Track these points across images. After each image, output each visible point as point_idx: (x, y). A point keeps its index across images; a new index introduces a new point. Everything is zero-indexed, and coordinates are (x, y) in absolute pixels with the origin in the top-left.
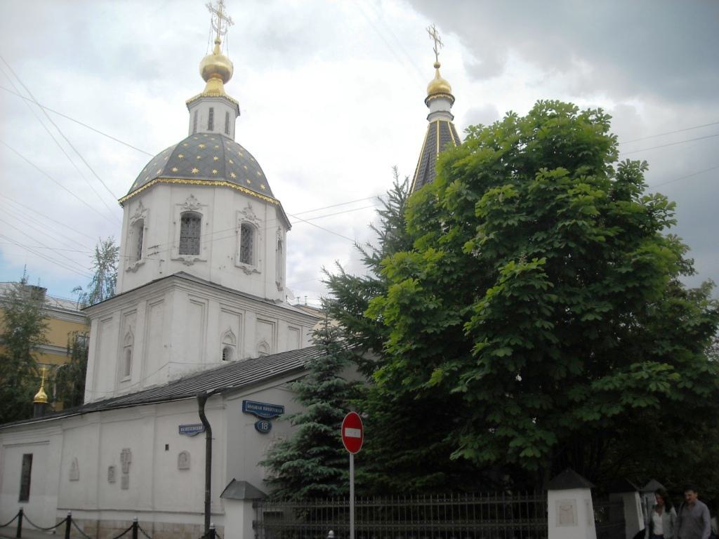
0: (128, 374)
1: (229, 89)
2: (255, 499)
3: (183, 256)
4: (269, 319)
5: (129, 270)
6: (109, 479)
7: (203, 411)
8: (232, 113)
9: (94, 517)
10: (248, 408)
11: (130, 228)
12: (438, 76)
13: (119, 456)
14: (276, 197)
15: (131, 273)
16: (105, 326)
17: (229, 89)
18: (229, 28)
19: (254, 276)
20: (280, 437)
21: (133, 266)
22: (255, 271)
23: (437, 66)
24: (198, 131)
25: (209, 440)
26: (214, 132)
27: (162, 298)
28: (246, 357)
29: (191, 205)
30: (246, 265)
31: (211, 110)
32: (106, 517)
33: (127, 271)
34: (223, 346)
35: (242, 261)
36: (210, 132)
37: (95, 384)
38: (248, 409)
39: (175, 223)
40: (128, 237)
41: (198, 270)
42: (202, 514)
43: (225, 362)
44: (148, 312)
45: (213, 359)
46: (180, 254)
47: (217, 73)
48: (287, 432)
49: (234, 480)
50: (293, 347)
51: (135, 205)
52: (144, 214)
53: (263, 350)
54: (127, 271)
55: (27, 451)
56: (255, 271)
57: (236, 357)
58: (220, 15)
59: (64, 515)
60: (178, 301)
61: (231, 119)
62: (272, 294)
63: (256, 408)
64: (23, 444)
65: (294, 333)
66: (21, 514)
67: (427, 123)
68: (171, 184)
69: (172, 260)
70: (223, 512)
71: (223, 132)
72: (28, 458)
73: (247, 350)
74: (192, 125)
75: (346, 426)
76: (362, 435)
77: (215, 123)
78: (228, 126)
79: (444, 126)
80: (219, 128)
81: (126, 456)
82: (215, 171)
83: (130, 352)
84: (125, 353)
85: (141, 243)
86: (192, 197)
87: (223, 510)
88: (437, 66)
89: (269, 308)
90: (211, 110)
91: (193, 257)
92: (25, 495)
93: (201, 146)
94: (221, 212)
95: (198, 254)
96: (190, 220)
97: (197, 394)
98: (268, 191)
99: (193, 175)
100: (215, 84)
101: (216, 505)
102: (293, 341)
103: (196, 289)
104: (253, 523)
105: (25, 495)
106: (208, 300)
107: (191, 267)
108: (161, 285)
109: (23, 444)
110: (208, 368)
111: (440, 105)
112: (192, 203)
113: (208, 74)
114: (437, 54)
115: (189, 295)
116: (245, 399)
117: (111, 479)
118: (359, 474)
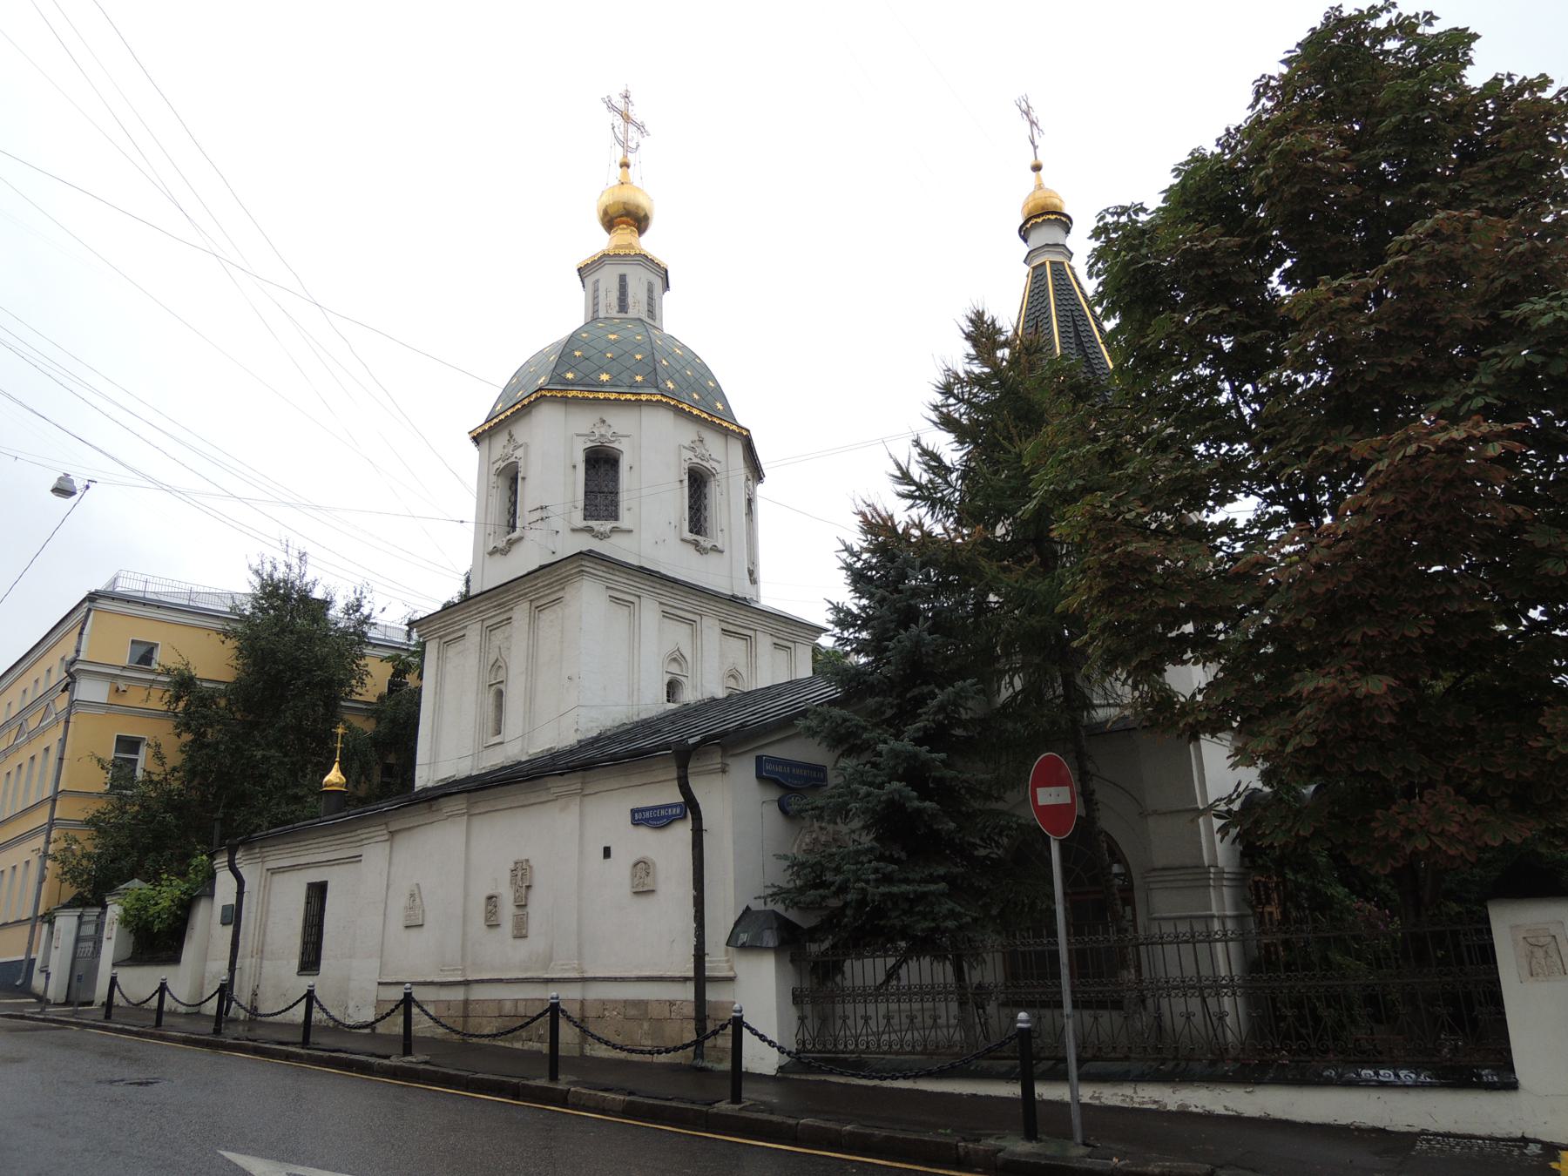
0: (498, 732)
1: (648, 243)
3: (595, 524)
4: (740, 631)
5: (495, 551)
7: (686, 777)
8: (658, 283)
9: (458, 995)
10: (767, 774)
11: (494, 478)
12: (1040, 187)
13: (508, 875)
14: (741, 422)
15: (498, 557)
16: (452, 652)
17: (648, 243)
18: (643, 142)
19: (713, 556)
21: (501, 544)
22: (715, 549)
23: (1037, 168)
24: (602, 314)
25: (698, 833)
28: (707, 695)
30: (699, 538)
31: (623, 278)
32: (478, 993)
33: (491, 554)
34: (667, 678)
35: (691, 531)
36: (622, 315)
40: (488, 495)
41: (615, 548)
42: (686, 979)
43: (672, 706)
44: (533, 621)
45: (651, 702)
47: (627, 217)
49: (748, 908)
50: (783, 678)
51: (501, 441)
52: (519, 453)
53: (732, 683)
54: (491, 554)
55: (315, 876)
56: (715, 549)
57: (689, 695)
58: (626, 118)
59: (397, 994)
60: (588, 600)
61: (656, 295)
62: (742, 589)
63: (780, 769)
64: (307, 866)
65: (783, 654)
67: (1027, 269)
68: (565, 401)
69: (574, 530)
70: (731, 974)
71: (644, 316)
72: (317, 893)
73: (706, 683)
75: (1037, 784)
76: (1073, 798)
77: (630, 300)
78: (652, 310)
80: (637, 308)
81: (522, 875)
82: (639, 378)
83: (500, 694)
84: (490, 698)
85: (514, 504)
86: (604, 422)
87: (731, 969)
89: (740, 612)
90: (623, 278)
91: (609, 525)
92: (310, 960)
93: (612, 337)
94: (654, 451)
95: (616, 518)
97: (661, 753)
98: (728, 413)
99: (603, 384)
100: (624, 236)
101: (718, 959)
102: (773, 668)
103: (620, 579)
105: (310, 960)
107: (606, 542)
108: (547, 581)
109: (307, 866)
110: (644, 716)
111: (1041, 237)
113: (611, 221)
114: (1035, 148)
116: (759, 753)
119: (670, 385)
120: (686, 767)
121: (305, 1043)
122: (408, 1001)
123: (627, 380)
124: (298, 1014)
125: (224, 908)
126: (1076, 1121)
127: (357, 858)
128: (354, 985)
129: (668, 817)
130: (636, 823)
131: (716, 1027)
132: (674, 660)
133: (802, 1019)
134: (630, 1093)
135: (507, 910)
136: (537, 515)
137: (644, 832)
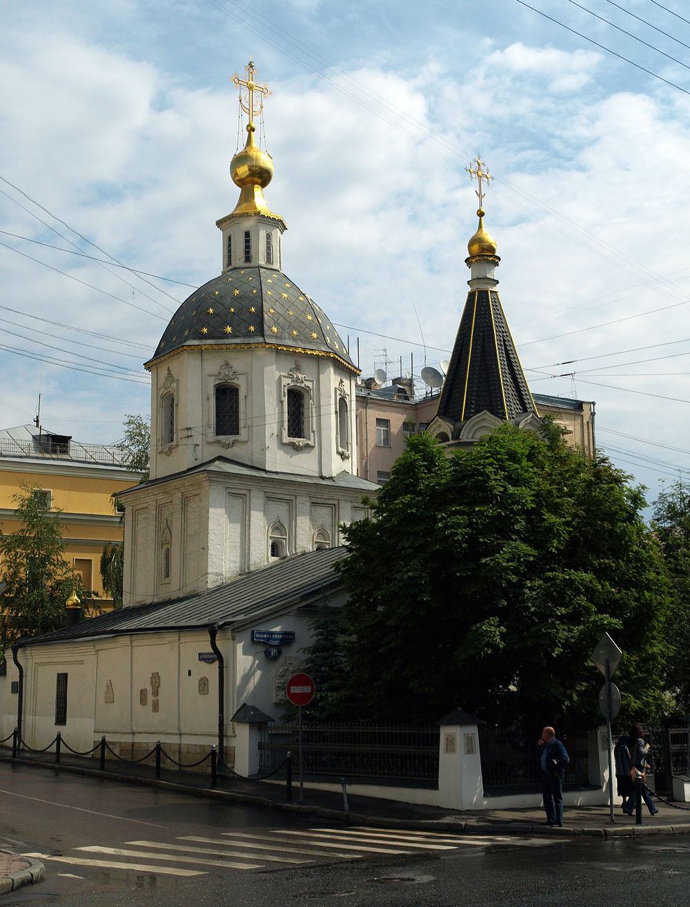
0: (167, 575)
3: (221, 437)
6: (141, 702)
9: (127, 739)
20: (292, 662)
25: (221, 668)
26: (252, 265)
27: (198, 492)
29: (226, 375)
30: (295, 440)
31: (63, 679)
32: (139, 739)
34: (270, 542)
36: (247, 265)
37: (133, 585)
38: (258, 638)
39: (208, 398)
46: (218, 434)
48: (295, 656)
49: (245, 704)
52: (174, 385)
55: (62, 669)
59: (99, 738)
65: (237, 503)
66: (59, 738)
72: (63, 679)
74: (226, 251)
79: (483, 295)
81: (155, 679)
88: (481, 214)
91: (232, 438)
92: (61, 719)
96: (227, 400)
104: (259, 743)
105: (61, 719)
106: (249, 490)
107: (230, 450)
112: (227, 373)
115: (226, 488)
117: (143, 701)
119: (275, 329)
120: (215, 637)
123: (243, 331)
124: (53, 749)
125: (13, 683)
126: (346, 801)
127: (81, 662)
128: (81, 733)
129: (212, 659)
130: (200, 659)
131: (220, 757)
132: (277, 528)
133: (261, 755)
134: (187, 785)
135: (150, 698)
136: (185, 433)
137: (203, 663)
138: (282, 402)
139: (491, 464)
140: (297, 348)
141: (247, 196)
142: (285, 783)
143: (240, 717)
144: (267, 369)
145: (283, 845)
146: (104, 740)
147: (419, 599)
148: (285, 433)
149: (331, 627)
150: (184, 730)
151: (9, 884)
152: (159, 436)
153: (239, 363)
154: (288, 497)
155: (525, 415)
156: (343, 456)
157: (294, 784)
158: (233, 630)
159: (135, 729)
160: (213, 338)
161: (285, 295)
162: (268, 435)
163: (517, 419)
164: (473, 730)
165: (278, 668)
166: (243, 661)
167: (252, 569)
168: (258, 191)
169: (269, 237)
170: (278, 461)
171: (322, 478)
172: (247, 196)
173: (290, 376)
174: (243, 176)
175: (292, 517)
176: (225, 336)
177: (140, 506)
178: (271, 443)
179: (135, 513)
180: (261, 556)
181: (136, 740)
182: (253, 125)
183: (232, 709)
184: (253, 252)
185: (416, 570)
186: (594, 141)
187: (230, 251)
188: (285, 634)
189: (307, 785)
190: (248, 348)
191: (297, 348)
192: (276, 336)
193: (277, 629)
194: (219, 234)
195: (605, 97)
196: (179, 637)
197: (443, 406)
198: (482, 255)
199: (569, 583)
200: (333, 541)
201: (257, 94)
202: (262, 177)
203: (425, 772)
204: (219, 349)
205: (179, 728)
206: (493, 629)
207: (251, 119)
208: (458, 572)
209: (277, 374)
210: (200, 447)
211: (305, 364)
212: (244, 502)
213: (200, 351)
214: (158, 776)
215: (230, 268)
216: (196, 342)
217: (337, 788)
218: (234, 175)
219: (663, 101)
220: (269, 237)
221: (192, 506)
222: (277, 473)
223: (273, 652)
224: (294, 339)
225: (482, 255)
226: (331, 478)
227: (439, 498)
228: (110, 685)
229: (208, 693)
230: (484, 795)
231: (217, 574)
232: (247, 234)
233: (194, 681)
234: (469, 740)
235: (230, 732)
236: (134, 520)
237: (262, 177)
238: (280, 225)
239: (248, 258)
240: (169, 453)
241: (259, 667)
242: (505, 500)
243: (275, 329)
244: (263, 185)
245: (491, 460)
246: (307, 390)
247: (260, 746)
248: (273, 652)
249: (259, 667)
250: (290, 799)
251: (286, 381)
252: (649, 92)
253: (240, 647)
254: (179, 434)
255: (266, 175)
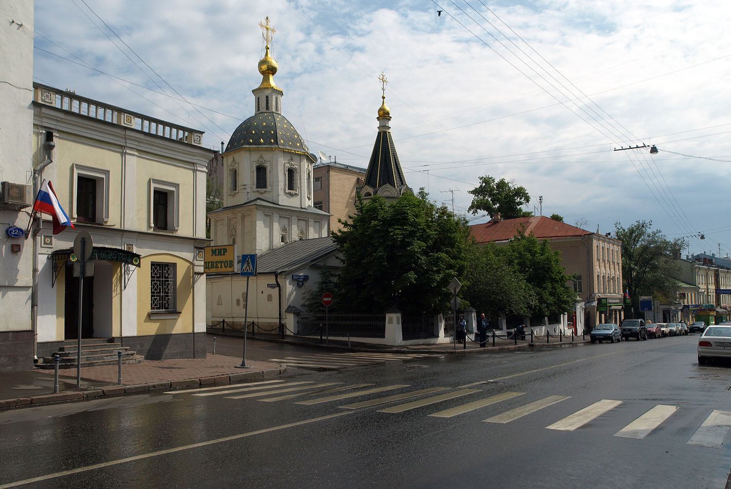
2: (297, 313)
9: (231, 320)
23: (384, 98)
27: (251, 213)
30: (291, 191)
32: (235, 320)
36: (267, 111)
46: (257, 188)
52: (237, 165)
65: (318, 224)
74: (257, 105)
79: (385, 133)
88: (384, 98)
91: (264, 190)
96: (261, 172)
118: (249, 336)
119: (282, 141)
121: (223, 332)
122: (224, 321)
131: (282, 327)
133: (298, 326)
136: (243, 187)
138: (285, 174)
139: (409, 209)
140: (292, 150)
141: (266, 79)
142: (319, 337)
143: (290, 309)
144: (279, 159)
145: (323, 359)
146: (224, 320)
147: (383, 264)
148: (287, 188)
149: (327, 274)
150: (259, 316)
151: (169, 383)
152: (229, 188)
153: (267, 156)
154: (288, 217)
155: (402, 186)
156: (309, 199)
157: (323, 338)
158: (285, 275)
159: (234, 316)
160: (255, 145)
161: (285, 126)
162: (280, 189)
163: (400, 188)
164: (399, 315)
165: (302, 290)
166: (289, 287)
167: (274, 248)
168: (271, 77)
169: (277, 98)
170: (284, 201)
171: (302, 208)
172: (266, 79)
173: (289, 163)
174: (264, 70)
175: (290, 225)
176: (260, 144)
177: (219, 219)
178: (281, 192)
179: (216, 221)
180: (277, 242)
181: (234, 321)
182: (269, 46)
183: (285, 307)
184: (270, 105)
185: (382, 252)
186: (369, 33)
187: (259, 104)
188: (305, 276)
189: (330, 338)
190: (272, 150)
191: (292, 150)
192: (283, 145)
193: (301, 274)
194: (253, 98)
195: (375, 10)
196: (231, 279)
197: (368, 180)
198: (384, 116)
199: (438, 258)
200: (306, 236)
201: (270, 32)
202: (273, 70)
203: (380, 332)
204: (258, 150)
205: (257, 316)
206: (412, 276)
207: (267, 44)
208: (398, 252)
209: (283, 162)
210: (250, 194)
211: (295, 157)
212: (271, 218)
213: (250, 150)
214: (253, 335)
215: (259, 112)
216: (248, 146)
217: (345, 339)
218: (260, 69)
219: (403, 15)
220: (277, 98)
221: (246, 220)
222: (284, 206)
223: (300, 283)
224: (290, 146)
225: (384, 116)
226: (305, 208)
227: (388, 223)
228: (220, 297)
229: (272, 301)
230: (445, 337)
231: (260, 250)
232: (267, 97)
233: (265, 295)
234: (398, 319)
235: (284, 317)
236: (216, 225)
237: (273, 70)
238: (281, 93)
239: (267, 108)
240: (234, 196)
241: (295, 290)
242: (414, 224)
243: (282, 141)
244: (273, 74)
245: (408, 208)
246: (296, 169)
247: (298, 322)
248: (300, 283)
249: (295, 290)
250: (322, 343)
251: (287, 165)
252: (397, 10)
253: (288, 282)
254: (239, 187)
255: (274, 70)
